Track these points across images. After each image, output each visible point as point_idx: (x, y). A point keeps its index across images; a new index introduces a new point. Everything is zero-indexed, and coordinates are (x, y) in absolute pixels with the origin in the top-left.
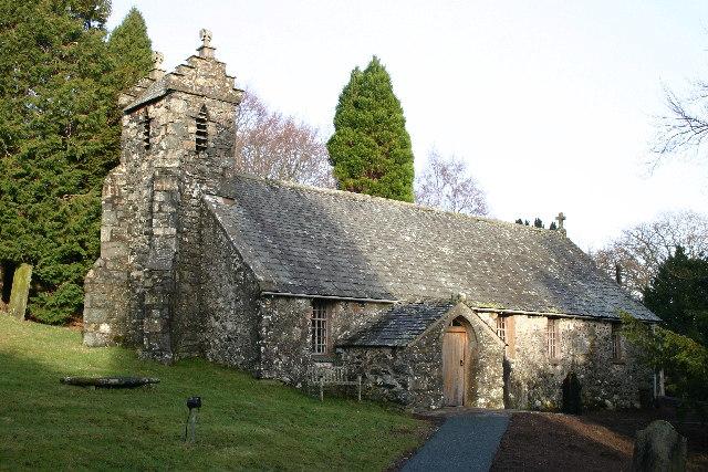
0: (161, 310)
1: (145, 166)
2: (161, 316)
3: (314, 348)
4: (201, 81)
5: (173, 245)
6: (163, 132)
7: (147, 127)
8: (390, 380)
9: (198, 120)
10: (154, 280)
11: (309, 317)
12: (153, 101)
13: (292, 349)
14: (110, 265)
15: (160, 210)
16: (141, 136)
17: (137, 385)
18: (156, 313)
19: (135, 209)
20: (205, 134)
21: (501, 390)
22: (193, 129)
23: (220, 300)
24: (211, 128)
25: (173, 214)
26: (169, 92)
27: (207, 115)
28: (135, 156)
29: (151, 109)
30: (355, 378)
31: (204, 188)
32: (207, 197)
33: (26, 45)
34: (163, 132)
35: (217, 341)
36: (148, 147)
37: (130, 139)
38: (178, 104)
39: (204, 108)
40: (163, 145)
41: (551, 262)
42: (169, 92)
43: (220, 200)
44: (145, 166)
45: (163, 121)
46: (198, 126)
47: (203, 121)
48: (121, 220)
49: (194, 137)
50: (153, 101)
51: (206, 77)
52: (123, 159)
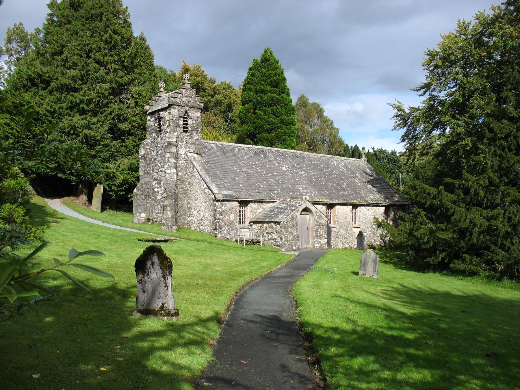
0: (171, 207)
1: (159, 139)
2: (171, 210)
3: (240, 222)
4: (184, 99)
5: (174, 177)
6: (167, 124)
7: (160, 121)
8: (275, 236)
9: (183, 118)
10: (168, 194)
11: (238, 209)
12: (164, 109)
13: (231, 224)
14: (144, 186)
15: (168, 161)
16: (156, 125)
17: (140, 240)
18: (169, 208)
19: (155, 159)
20: (187, 124)
21: (326, 240)
22: (181, 122)
23: (197, 202)
24: (190, 122)
25: (174, 163)
26: (170, 106)
27: (188, 115)
28: (154, 135)
29: (161, 113)
30: (259, 236)
31: (188, 149)
32: (189, 154)
33: (297, 304)
34: (167, 124)
35: (196, 221)
36: (160, 131)
37: (151, 126)
38: (174, 111)
39: (186, 112)
40: (168, 130)
41: (357, 177)
42: (170, 106)
43: (195, 155)
44: (159, 139)
45: (167, 119)
46: (184, 121)
47: (186, 118)
48: (148, 164)
49: (182, 126)
50: (164, 109)
51: (187, 97)
52: (148, 136)
